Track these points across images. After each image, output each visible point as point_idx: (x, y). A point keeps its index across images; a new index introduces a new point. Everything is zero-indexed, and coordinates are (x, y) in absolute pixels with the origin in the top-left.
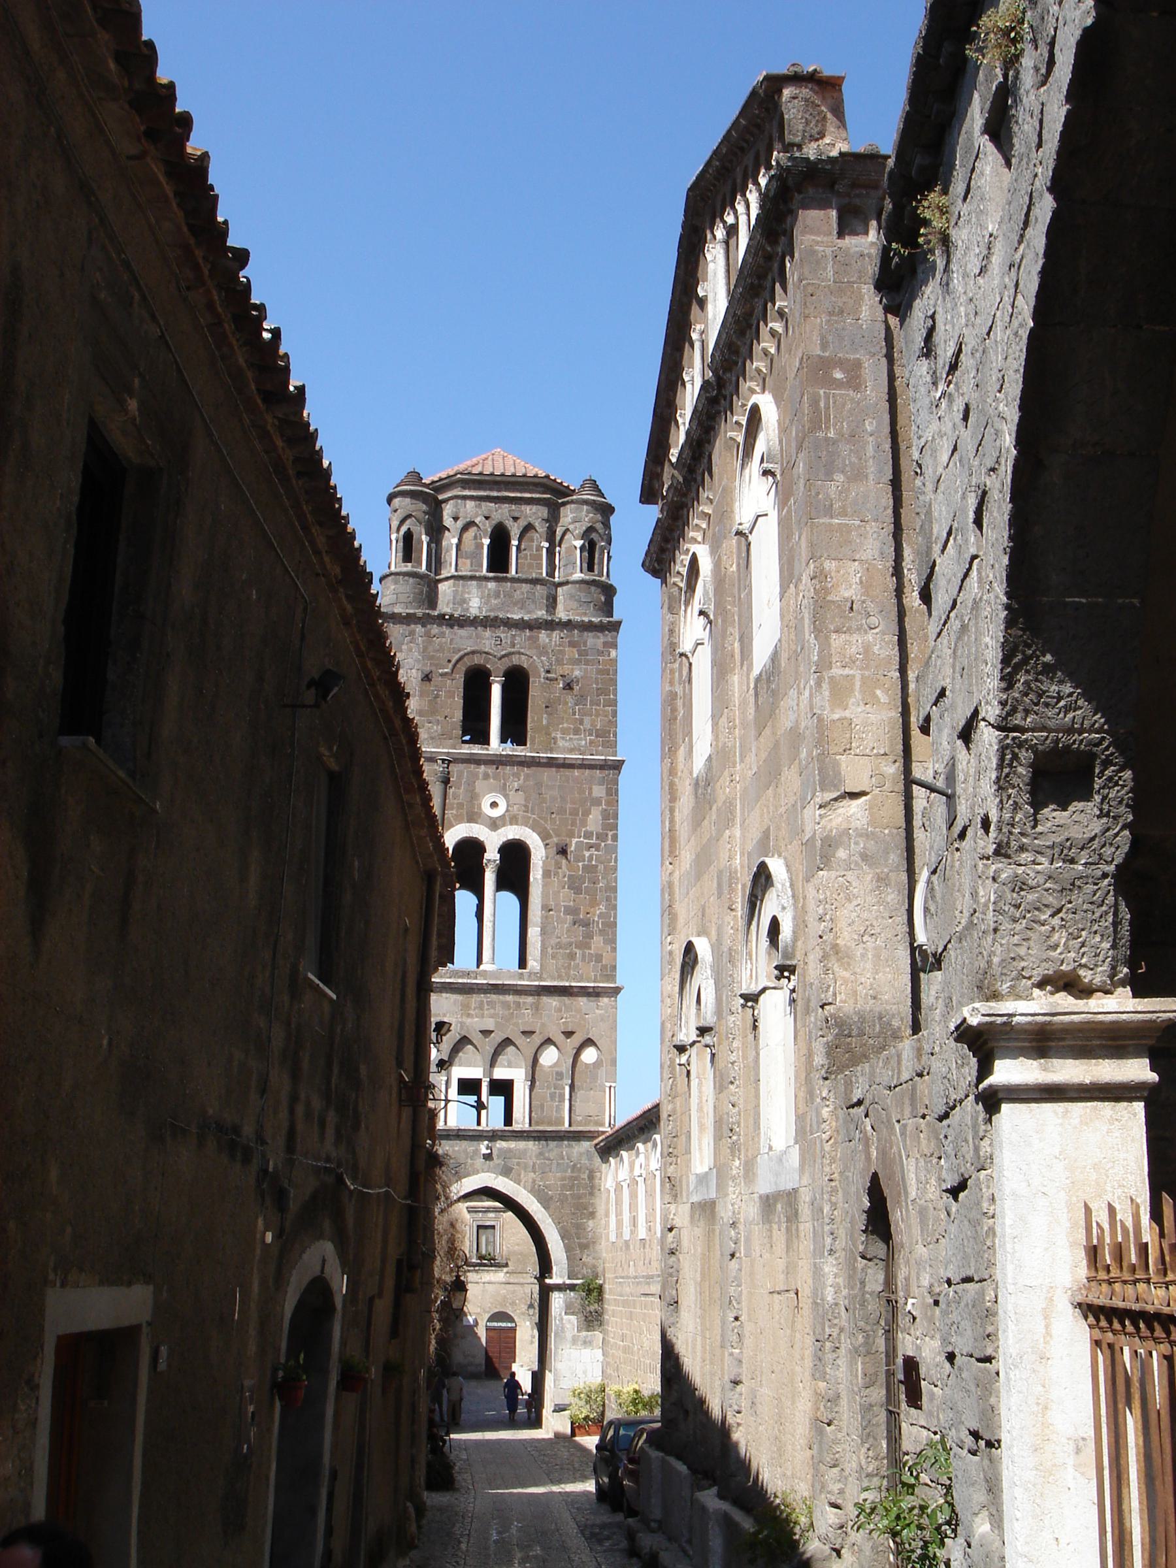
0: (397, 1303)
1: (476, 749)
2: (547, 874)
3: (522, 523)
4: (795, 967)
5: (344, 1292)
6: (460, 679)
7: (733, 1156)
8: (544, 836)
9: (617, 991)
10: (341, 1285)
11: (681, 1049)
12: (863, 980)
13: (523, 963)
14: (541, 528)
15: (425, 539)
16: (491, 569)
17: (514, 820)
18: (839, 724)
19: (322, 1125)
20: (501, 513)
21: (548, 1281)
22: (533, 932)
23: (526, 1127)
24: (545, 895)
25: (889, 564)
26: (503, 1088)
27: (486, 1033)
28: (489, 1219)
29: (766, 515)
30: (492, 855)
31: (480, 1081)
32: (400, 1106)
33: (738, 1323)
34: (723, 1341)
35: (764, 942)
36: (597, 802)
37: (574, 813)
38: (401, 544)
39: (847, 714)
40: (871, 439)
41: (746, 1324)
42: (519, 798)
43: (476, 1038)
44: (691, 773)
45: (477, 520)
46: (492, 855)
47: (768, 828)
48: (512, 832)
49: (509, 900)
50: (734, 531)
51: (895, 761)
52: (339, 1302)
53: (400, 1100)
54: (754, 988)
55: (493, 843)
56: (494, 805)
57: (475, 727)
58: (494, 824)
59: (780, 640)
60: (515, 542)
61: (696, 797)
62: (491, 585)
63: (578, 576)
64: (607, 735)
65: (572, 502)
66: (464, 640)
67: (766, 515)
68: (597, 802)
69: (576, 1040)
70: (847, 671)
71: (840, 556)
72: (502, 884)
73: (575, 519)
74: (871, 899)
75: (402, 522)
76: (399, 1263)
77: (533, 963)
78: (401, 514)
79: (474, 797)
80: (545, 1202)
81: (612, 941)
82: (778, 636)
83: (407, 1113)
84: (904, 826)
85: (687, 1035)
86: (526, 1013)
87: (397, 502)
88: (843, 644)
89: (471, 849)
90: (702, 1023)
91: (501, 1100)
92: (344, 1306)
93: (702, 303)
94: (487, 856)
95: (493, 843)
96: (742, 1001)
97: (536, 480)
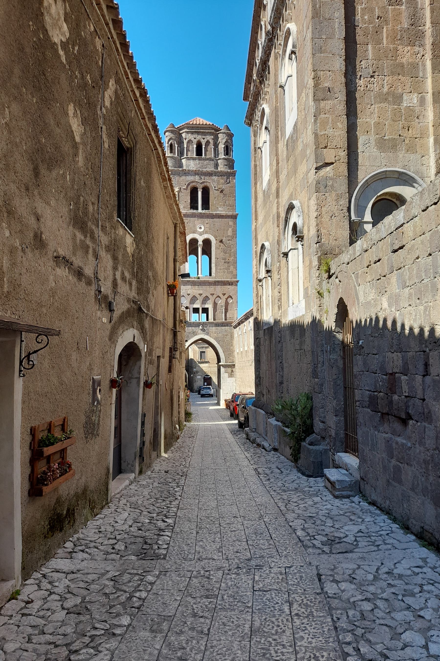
0: (170, 361)
1: (195, 211)
2: (216, 248)
3: (206, 140)
4: (303, 236)
5: (145, 351)
6: (189, 191)
7: (279, 310)
8: (215, 237)
9: (238, 282)
10: (143, 348)
11: (260, 281)
12: (331, 233)
13: (210, 274)
14: (211, 142)
15: (176, 145)
16: (197, 155)
17: (206, 233)
18: (323, 136)
19: (131, 284)
20: (199, 137)
21: (220, 364)
22: (213, 265)
23: (212, 321)
24: (216, 255)
25: (343, 72)
26: (205, 311)
27: (200, 295)
28: (204, 350)
29: (291, 76)
30: (200, 243)
31: (199, 308)
32: (168, 296)
33: (281, 364)
34: (276, 370)
35: (290, 232)
36: (230, 226)
37: (224, 230)
38: (169, 148)
39: (326, 132)
40: (337, 20)
41: (284, 364)
42: (207, 226)
43: (198, 296)
44: (262, 189)
45: (192, 139)
46: (200, 243)
47: (292, 193)
48: (206, 236)
49: (206, 258)
50: (279, 86)
51: (344, 151)
52: (143, 355)
53: (168, 294)
54: (286, 251)
55: (200, 239)
56: (200, 228)
57: (194, 205)
58: (201, 234)
59: (297, 119)
60: (204, 146)
61: (264, 196)
62: (197, 161)
63: (224, 157)
64: (233, 206)
65: (221, 133)
66: (190, 178)
67: (291, 76)
68: (230, 226)
69: (226, 296)
70: (326, 116)
71: (324, 69)
72: (204, 253)
73: (222, 139)
74: (334, 203)
75: (169, 140)
76: (171, 349)
77: (213, 274)
78: (168, 138)
79: (195, 226)
80: (218, 342)
81: (236, 268)
82: (296, 118)
83: (172, 298)
84: (347, 175)
85: (262, 276)
86: (211, 289)
87: (167, 134)
88: (326, 105)
89: (194, 242)
90: (267, 269)
91: (205, 315)
92: (146, 356)
93: (265, 7)
94: (199, 243)
95: (200, 239)
96: (283, 255)
97: (210, 126)
